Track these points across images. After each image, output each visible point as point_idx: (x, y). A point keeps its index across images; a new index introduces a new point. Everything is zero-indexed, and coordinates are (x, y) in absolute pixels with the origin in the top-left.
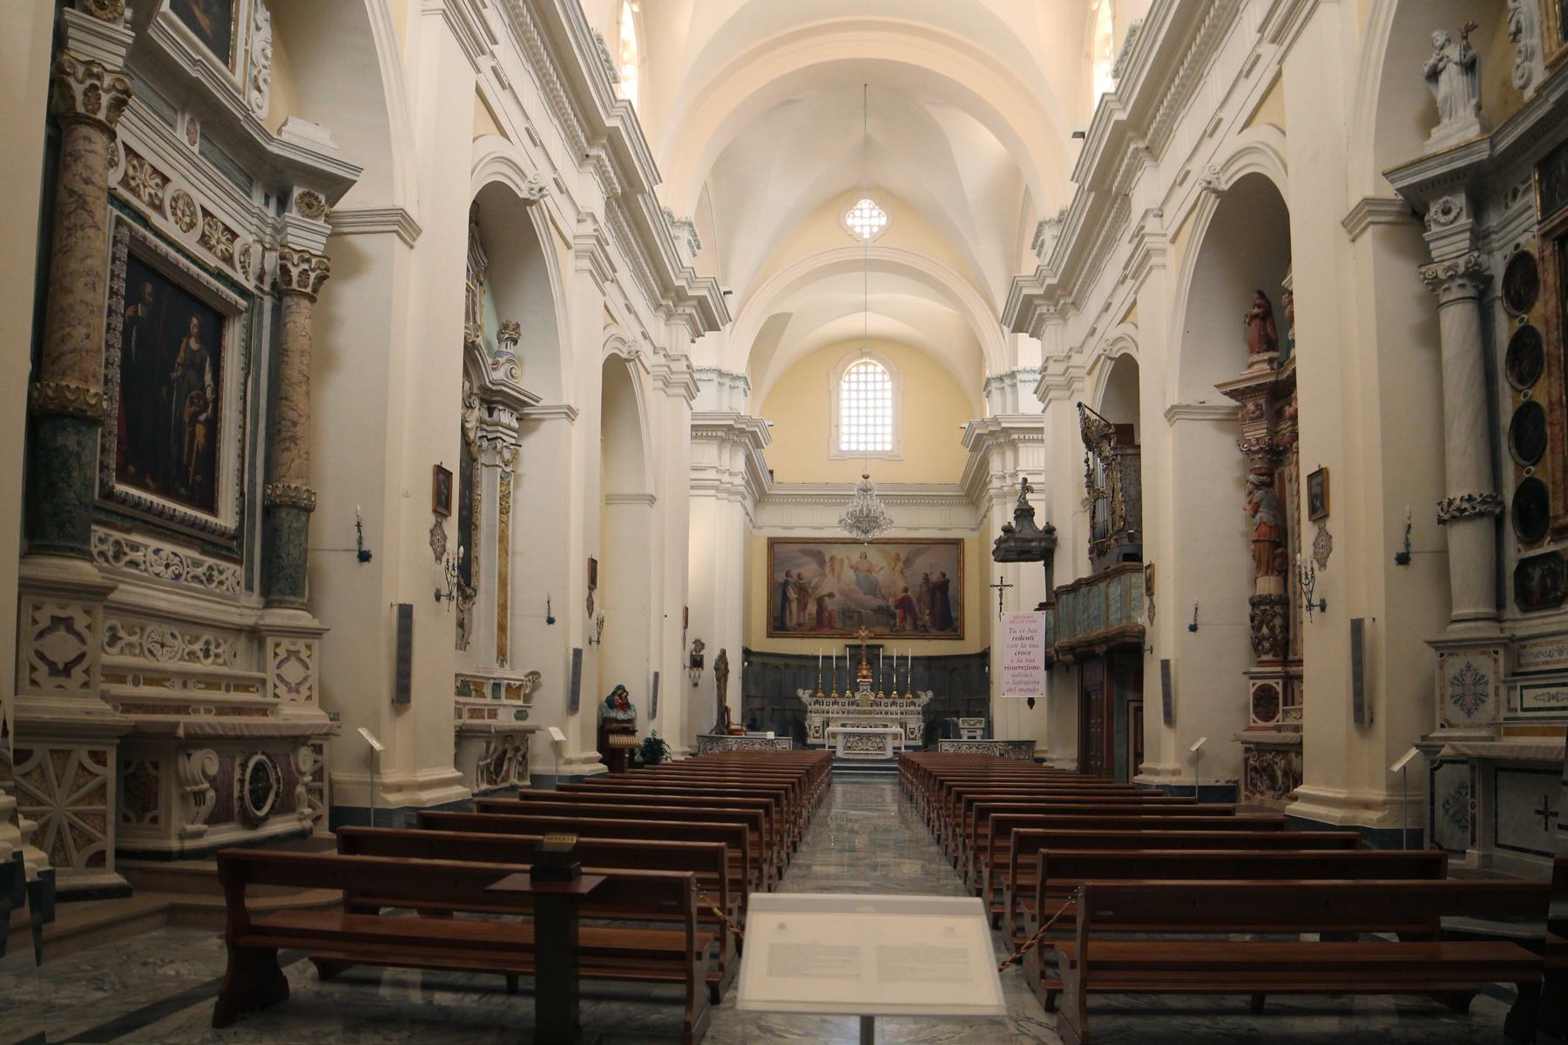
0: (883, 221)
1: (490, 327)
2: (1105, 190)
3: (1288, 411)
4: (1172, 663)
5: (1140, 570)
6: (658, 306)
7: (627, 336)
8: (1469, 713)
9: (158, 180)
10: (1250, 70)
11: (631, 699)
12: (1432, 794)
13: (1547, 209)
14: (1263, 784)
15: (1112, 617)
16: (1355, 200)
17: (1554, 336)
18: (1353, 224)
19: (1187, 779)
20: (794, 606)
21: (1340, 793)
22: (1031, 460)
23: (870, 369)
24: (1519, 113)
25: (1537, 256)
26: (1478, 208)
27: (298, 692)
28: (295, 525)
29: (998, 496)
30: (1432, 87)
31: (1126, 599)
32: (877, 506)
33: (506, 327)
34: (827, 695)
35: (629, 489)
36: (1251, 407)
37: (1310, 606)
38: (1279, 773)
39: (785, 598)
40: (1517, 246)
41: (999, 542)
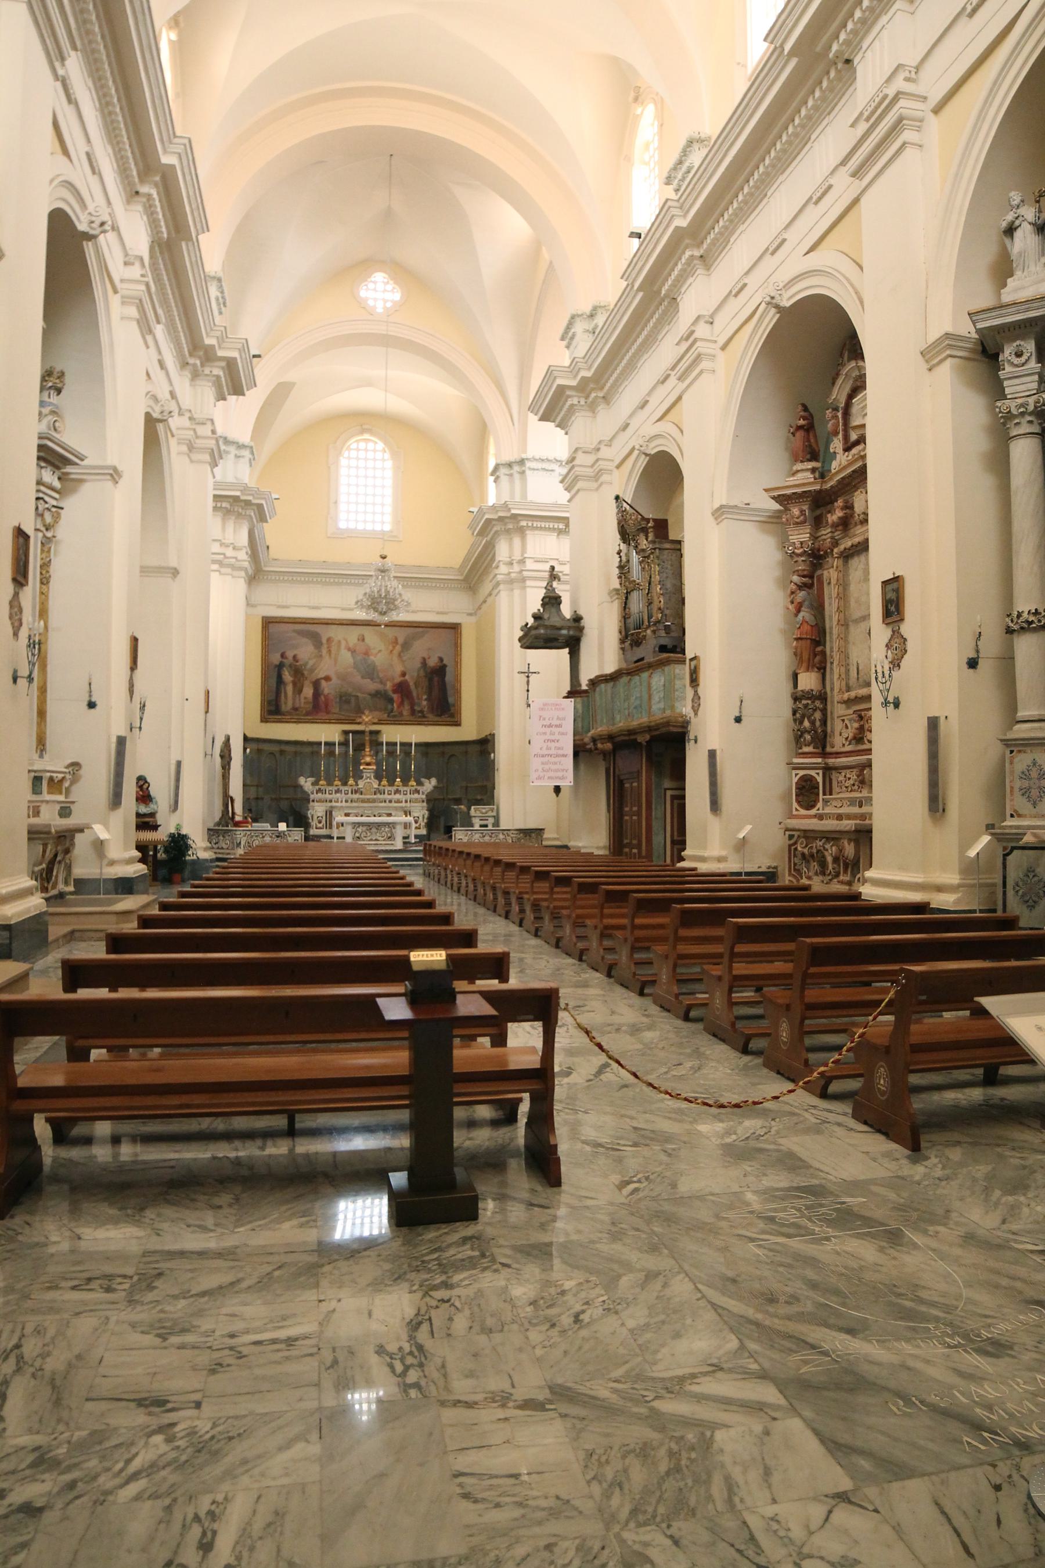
0: (397, 296)
2: (653, 295)
4: (718, 753)
5: (683, 662)
6: (184, 364)
8: (1035, 805)
10: (820, 199)
11: (153, 791)
12: (1005, 877)
15: (654, 707)
16: (934, 334)
18: (931, 355)
19: (732, 866)
20: (290, 688)
22: (544, 549)
23: (371, 446)
29: (505, 582)
30: (1007, 241)
31: (669, 691)
32: (394, 586)
34: (330, 783)
36: (796, 511)
38: (829, 859)
39: (280, 681)
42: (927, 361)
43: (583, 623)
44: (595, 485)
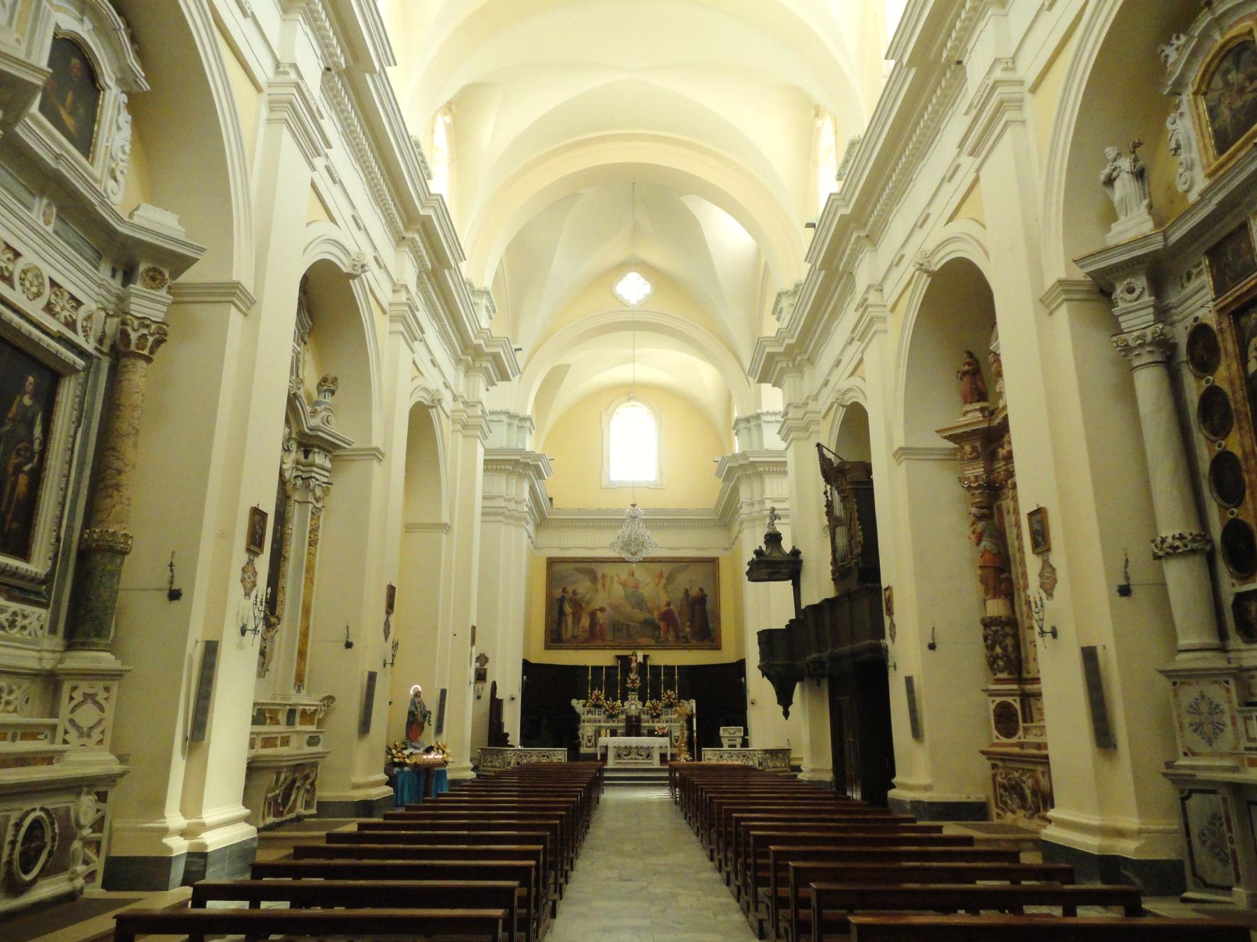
1: (311, 377)
3: (1002, 452)
4: (915, 679)
6: (458, 361)
7: (432, 387)
9: (10, 255)
13: (1220, 289)
14: (1014, 802)
16: (1050, 282)
17: (1240, 394)
20: (570, 619)
21: (1094, 820)
22: (777, 490)
24: (1183, 215)
25: (1215, 327)
26: (1158, 286)
27: (89, 736)
28: (109, 568)
30: (1107, 191)
33: (325, 380)
35: (424, 520)
36: (968, 448)
37: (1042, 633)
39: (561, 613)
40: (1196, 319)
41: (751, 563)
42: (1047, 307)
43: (802, 556)
44: (806, 435)
